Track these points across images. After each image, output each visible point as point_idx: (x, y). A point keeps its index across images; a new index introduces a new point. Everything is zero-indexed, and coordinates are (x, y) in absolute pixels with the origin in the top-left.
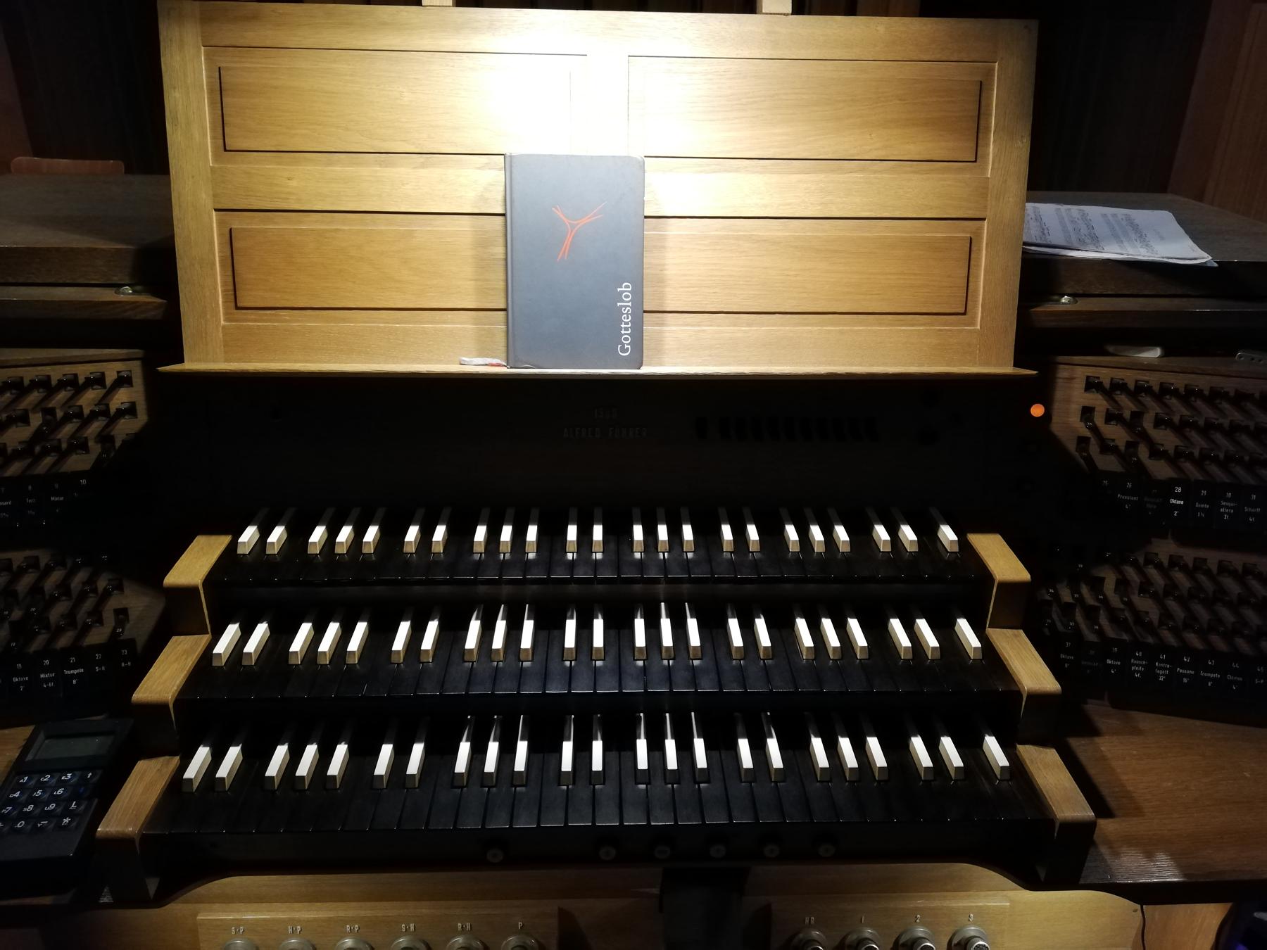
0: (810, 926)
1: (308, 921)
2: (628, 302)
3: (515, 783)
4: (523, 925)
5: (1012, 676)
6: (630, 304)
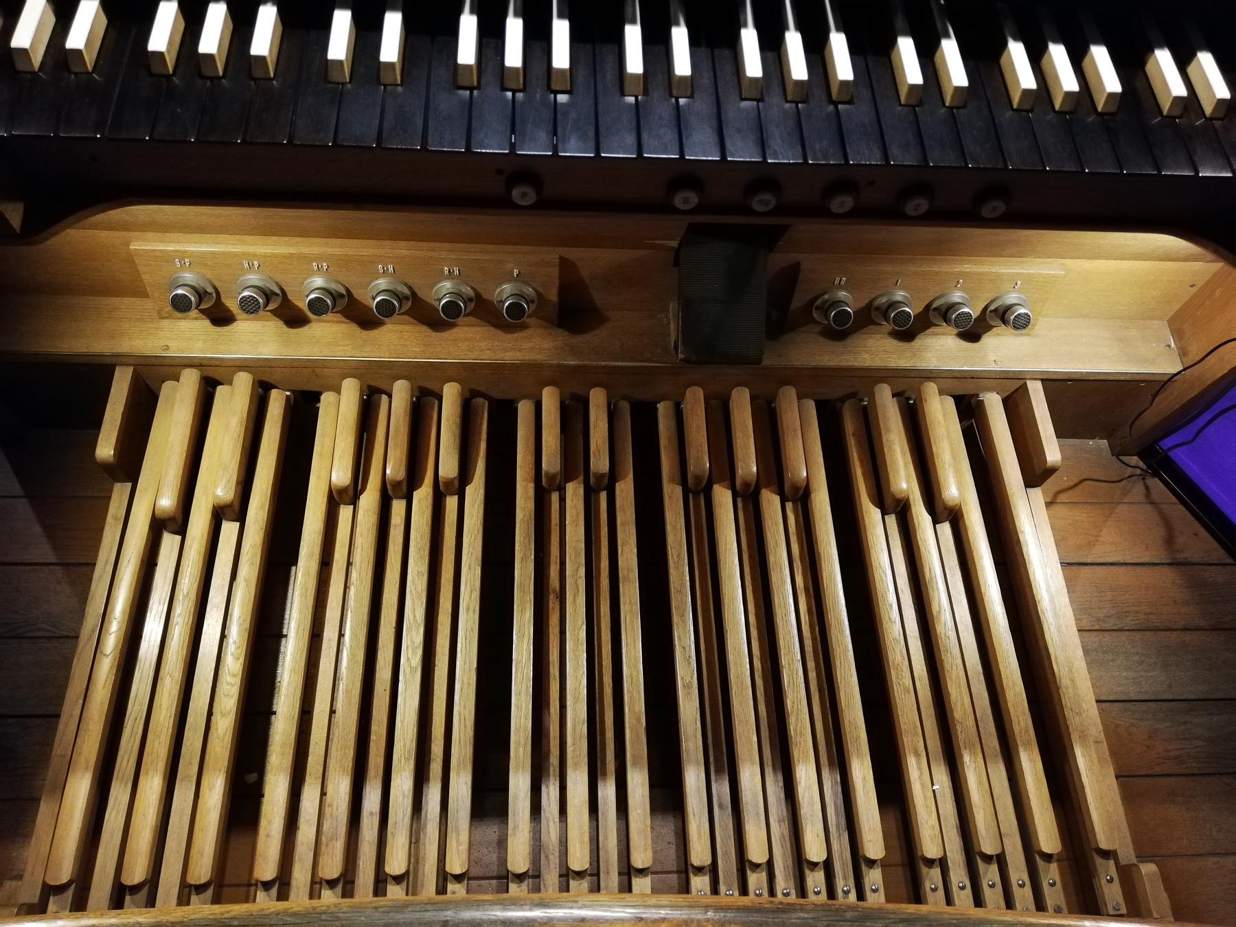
0: (840, 287)
1: (265, 256)
3: (554, 87)
4: (519, 273)
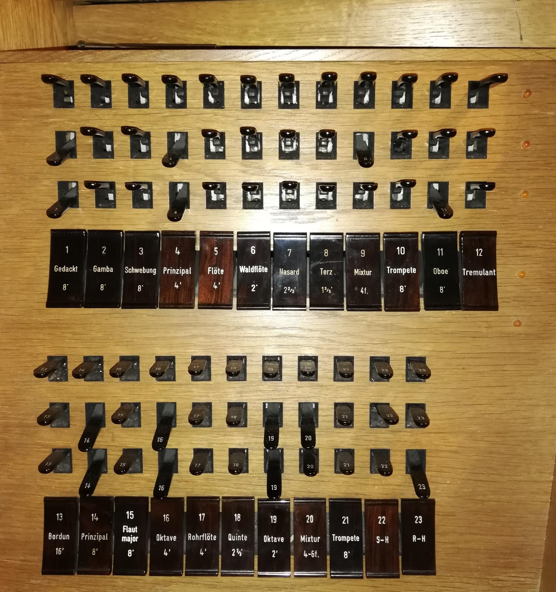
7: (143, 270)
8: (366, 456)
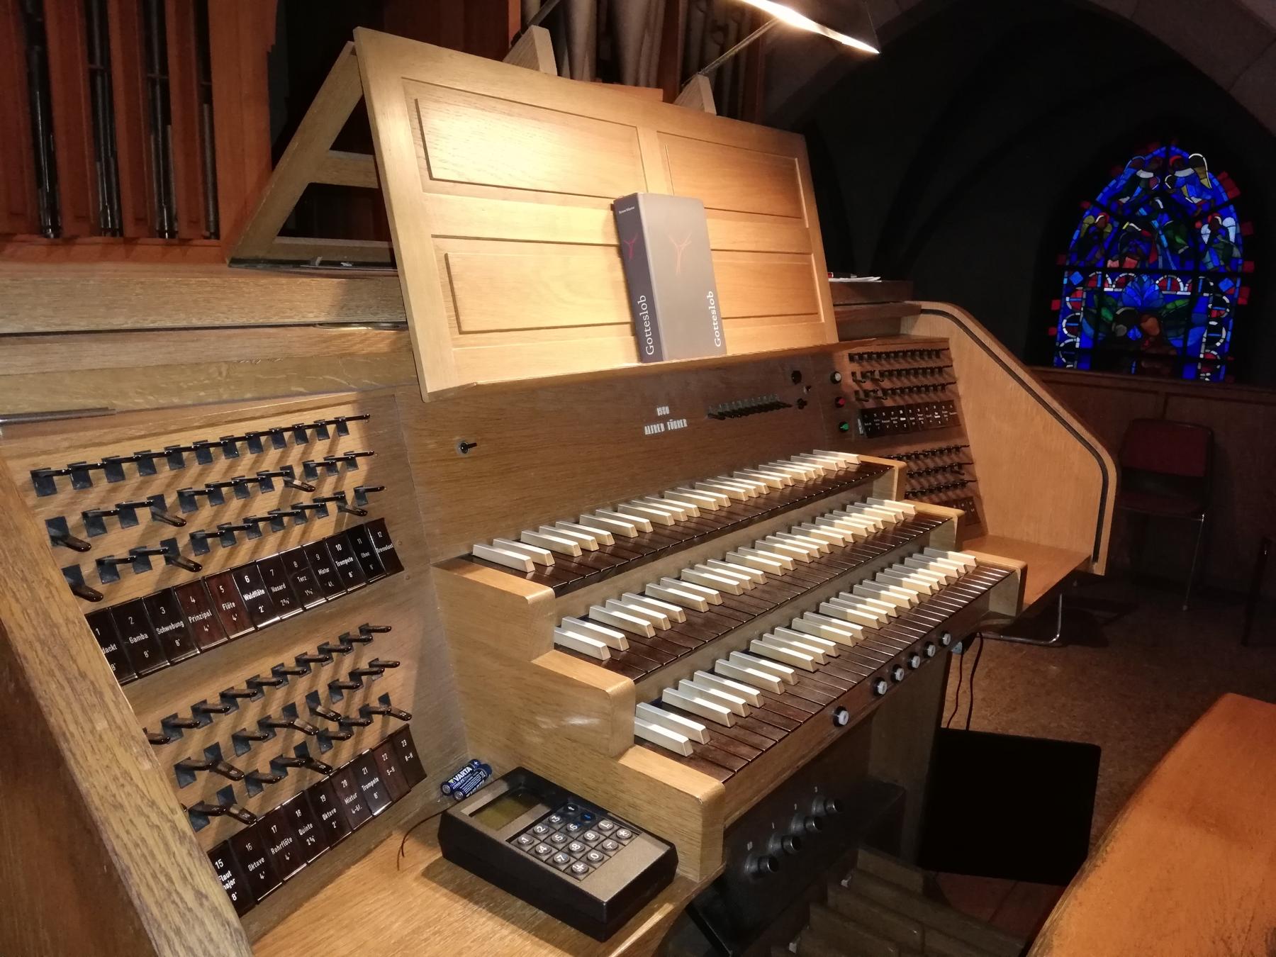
2: (646, 311)
5: (1018, 358)
6: (647, 312)
7: (172, 627)
8: (393, 532)
